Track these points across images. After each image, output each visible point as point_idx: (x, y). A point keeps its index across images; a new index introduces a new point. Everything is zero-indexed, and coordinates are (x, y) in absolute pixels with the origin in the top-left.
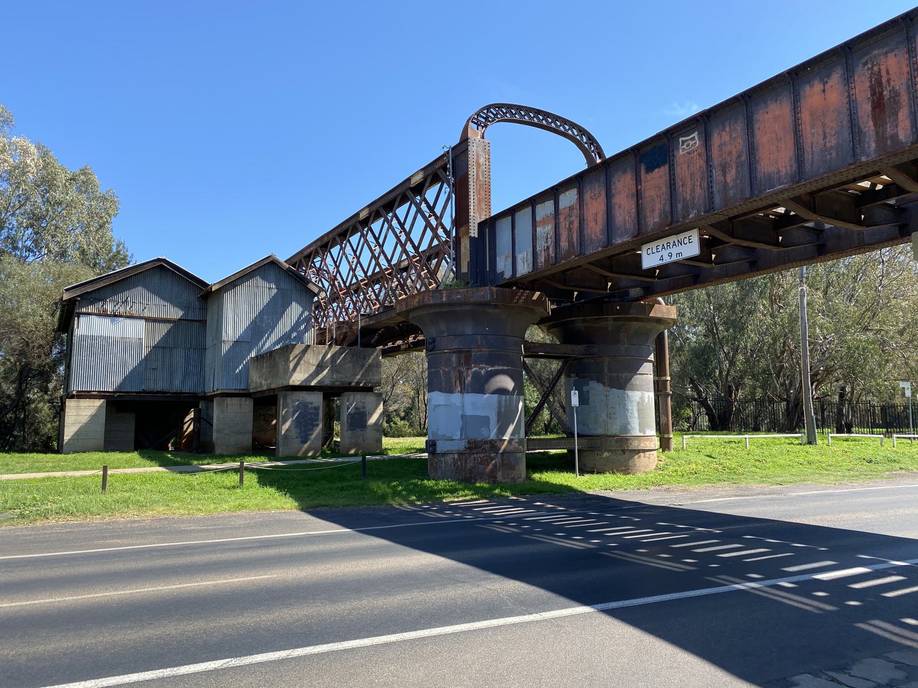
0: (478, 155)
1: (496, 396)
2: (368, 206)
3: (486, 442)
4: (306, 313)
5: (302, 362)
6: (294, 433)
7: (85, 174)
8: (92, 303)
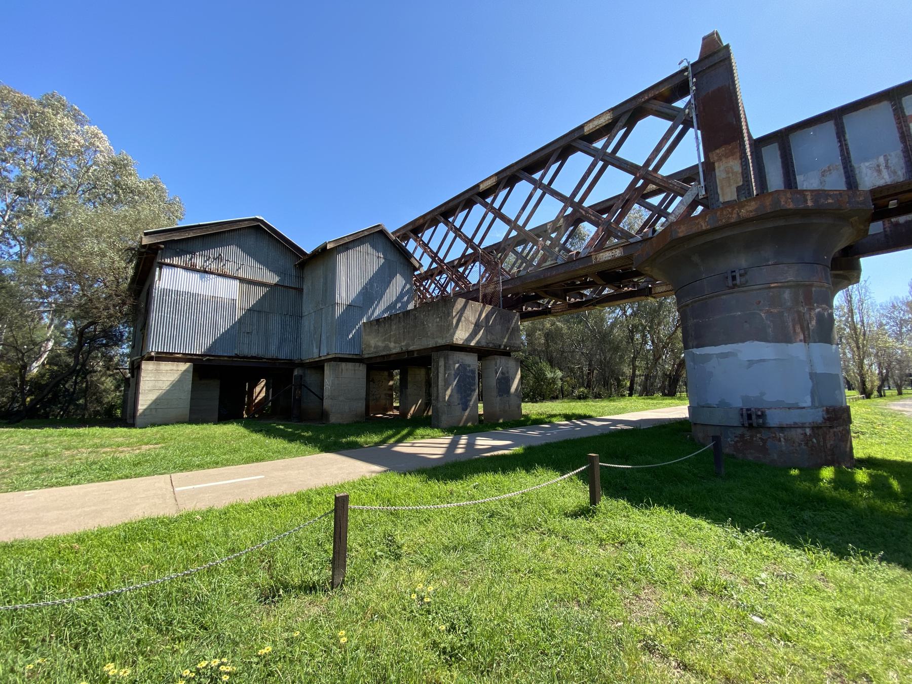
2: (496, 174)
4: (408, 286)
6: (456, 399)
8: (178, 254)
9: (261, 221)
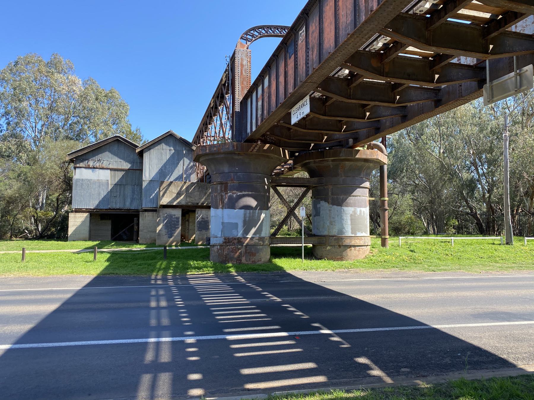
0: (242, 59)
1: (243, 210)
2: (213, 98)
3: (235, 239)
5: (168, 191)
6: (164, 232)
7: (111, 93)
8: (82, 161)
9: (119, 137)
